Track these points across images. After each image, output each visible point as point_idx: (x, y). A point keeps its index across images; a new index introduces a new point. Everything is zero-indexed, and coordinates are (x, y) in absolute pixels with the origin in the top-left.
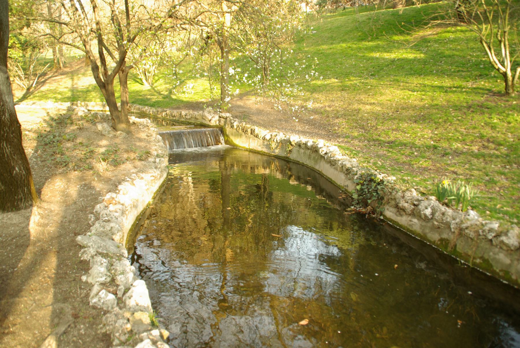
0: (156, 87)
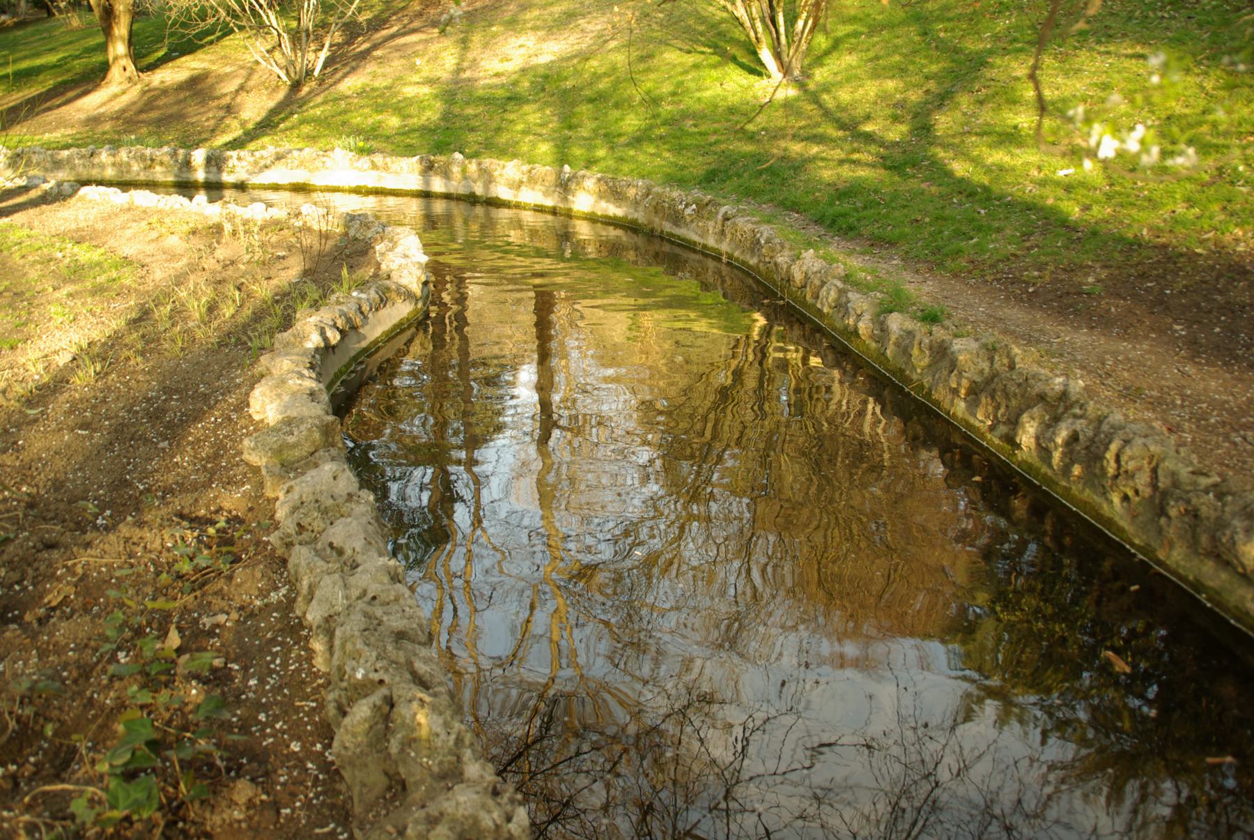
0: (826, 88)
